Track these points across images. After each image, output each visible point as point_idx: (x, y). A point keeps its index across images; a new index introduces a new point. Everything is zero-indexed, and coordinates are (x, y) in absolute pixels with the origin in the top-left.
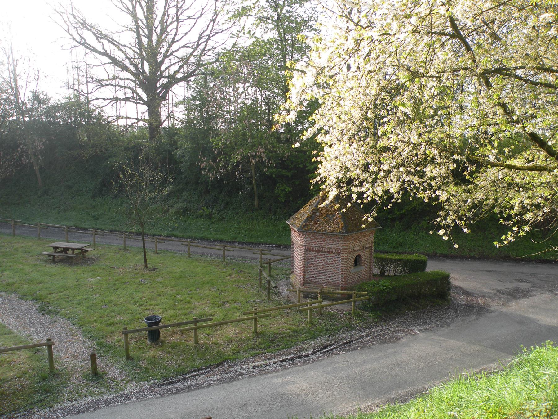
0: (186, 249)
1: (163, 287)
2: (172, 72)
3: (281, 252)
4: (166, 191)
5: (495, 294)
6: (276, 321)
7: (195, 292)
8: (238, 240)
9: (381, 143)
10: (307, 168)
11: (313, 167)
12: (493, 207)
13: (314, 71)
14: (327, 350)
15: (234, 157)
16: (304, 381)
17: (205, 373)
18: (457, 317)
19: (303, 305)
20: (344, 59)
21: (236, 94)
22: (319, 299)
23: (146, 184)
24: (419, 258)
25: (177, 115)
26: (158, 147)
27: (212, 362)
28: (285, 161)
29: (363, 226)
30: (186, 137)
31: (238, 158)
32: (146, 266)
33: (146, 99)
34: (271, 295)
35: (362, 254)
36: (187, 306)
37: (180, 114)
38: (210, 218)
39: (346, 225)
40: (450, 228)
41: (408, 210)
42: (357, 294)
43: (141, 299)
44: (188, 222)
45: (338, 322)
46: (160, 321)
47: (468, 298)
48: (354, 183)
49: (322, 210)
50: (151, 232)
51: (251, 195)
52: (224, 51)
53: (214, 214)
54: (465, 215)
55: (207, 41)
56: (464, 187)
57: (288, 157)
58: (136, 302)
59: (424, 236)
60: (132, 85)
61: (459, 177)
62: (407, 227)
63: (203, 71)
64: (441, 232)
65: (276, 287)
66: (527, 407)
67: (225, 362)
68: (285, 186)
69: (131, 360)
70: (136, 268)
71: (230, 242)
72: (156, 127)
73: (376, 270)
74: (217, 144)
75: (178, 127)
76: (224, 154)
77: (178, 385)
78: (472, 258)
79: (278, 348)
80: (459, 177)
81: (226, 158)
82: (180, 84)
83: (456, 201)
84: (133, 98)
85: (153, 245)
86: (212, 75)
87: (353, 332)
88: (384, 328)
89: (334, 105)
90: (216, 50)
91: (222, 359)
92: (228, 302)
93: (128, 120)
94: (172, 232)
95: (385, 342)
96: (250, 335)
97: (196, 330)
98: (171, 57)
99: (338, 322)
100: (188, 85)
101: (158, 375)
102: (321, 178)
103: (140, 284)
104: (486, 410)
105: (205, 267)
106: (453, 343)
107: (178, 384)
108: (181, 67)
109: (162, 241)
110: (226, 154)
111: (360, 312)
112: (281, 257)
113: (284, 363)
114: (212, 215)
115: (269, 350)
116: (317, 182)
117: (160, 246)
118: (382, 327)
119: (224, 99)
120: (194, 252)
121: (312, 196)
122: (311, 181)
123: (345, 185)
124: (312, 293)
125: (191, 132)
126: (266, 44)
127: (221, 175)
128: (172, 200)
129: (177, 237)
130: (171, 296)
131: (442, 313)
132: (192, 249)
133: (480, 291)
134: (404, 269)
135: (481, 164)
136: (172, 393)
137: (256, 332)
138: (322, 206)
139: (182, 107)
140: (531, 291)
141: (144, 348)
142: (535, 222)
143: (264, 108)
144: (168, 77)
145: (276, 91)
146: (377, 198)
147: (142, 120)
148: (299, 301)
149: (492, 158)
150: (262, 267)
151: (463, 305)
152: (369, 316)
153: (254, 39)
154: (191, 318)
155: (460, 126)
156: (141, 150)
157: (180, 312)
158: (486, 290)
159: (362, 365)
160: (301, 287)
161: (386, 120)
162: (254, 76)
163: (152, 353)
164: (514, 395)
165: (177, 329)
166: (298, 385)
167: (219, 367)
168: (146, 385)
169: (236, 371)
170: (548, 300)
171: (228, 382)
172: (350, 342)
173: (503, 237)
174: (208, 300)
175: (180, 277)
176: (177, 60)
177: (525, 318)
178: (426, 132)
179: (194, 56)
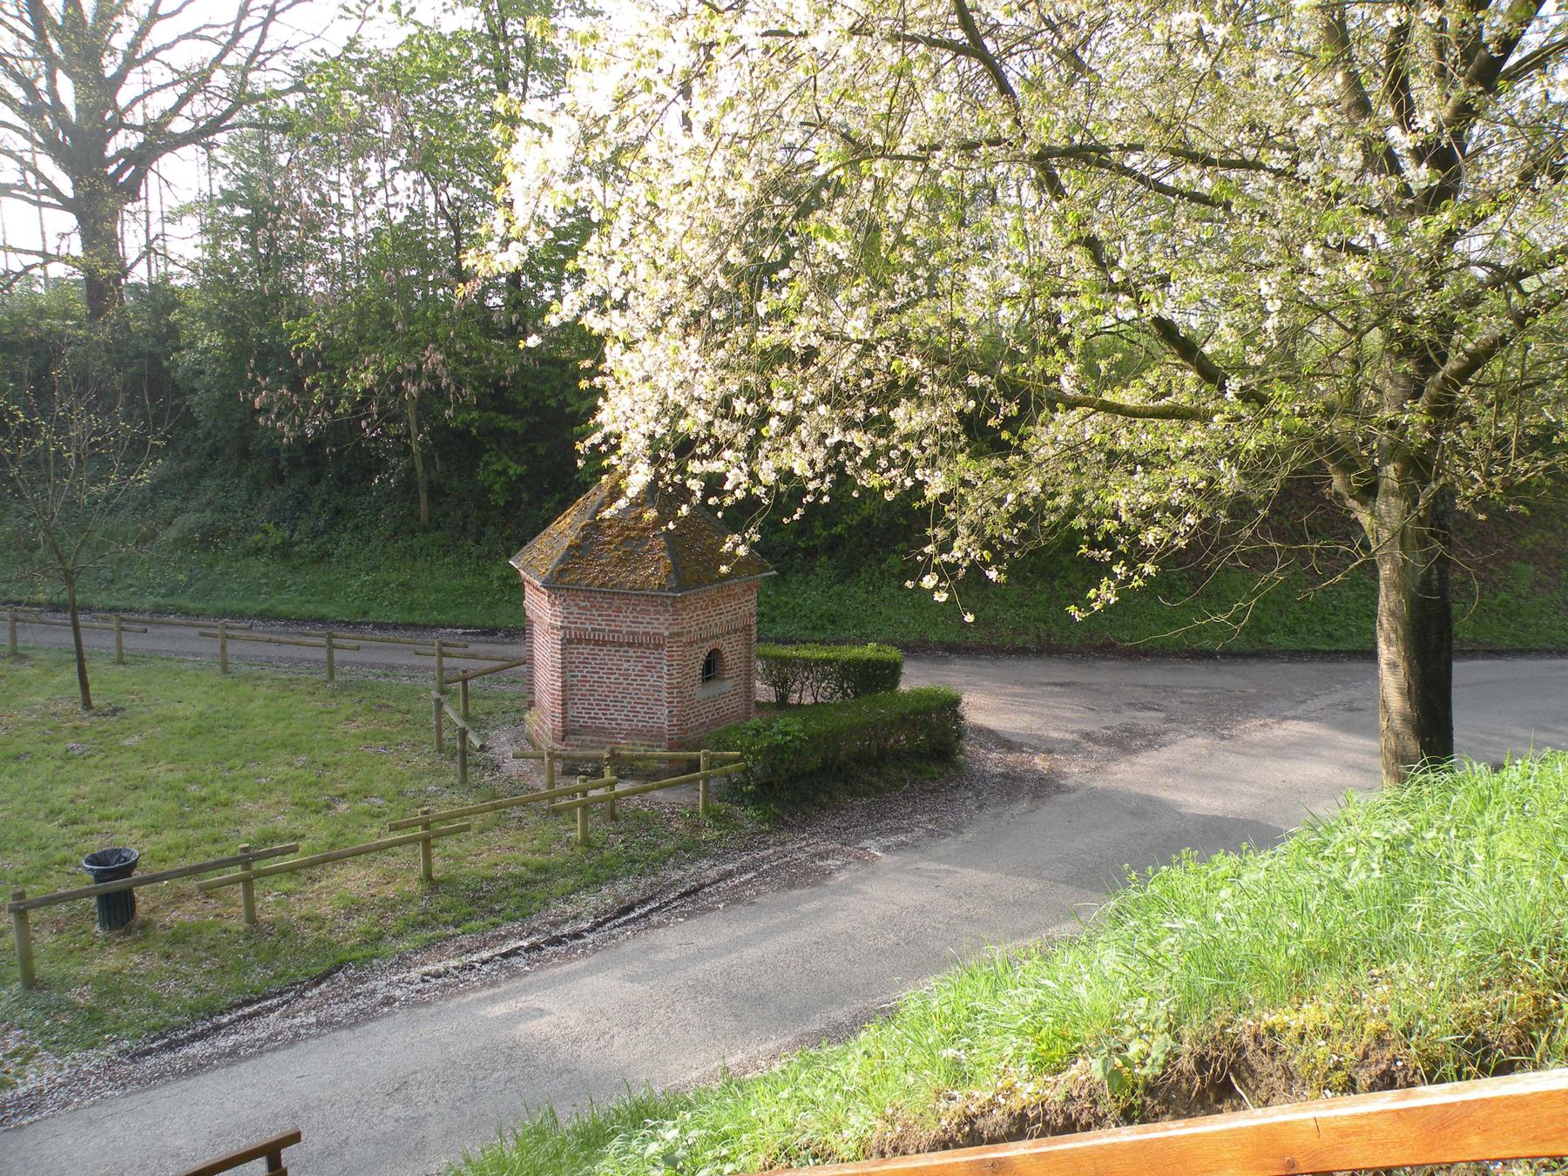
0: (214, 647)
1: (145, 762)
2: (154, 114)
3: (498, 648)
4: (145, 477)
5: (1076, 744)
6: (489, 843)
7: (245, 772)
8: (372, 616)
9: (766, 338)
10: (568, 410)
11: (586, 405)
12: (1072, 513)
13: (574, 126)
14: (633, 915)
15: (356, 378)
16: (586, 1009)
17: (279, 1006)
18: (980, 808)
19: (562, 794)
20: (664, 97)
21: (358, 192)
22: (608, 775)
23: (78, 455)
24: (881, 655)
25: (175, 247)
26: (117, 342)
27: (301, 973)
28: (505, 388)
29: (724, 569)
30: (206, 315)
31: (368, 378)
32: (87, 704)
33: (70, 194)
34: (469, 770)
35: (726, 649)
36: (221, 814)
37: (186, 244)
38: (286, 556)
39: (677, 569)
40: (962, 572)
41: (850, 527)
42: (712, 758)
43: (72, 801)
44: (218, 569)
45: (664, 837)
46: (134, 865)
47: (1011, 758)
48: (698, 451)
49: (610, 527)
50: (101, 599)
51: (408, 485)
52: (320, 60)
53: (297, 544)
54: (1001, 537)
55: (265, 24)
56: (996, 463)
57: (514, 377)
58: (54, 813)
59: (893, 596)
60: (19, 143)
61: (979, 436)
62: (848, 573)
63: (256, 115)
64: (929, 581)
65: (482, 748)
66: (1126, 1016)
67: (339, 969)
68: (506, 459)
69: (40, 989)
70: (52, 709)
71: (349, 623)
72: (107, 281)
73: (764, 691)
74: (307, 336)
75: (180, 283)
76: (325, 367)
77: (197, 1049)
78: (1021, 652)
79: (492, 919)
80: (979, 436)
81: (330, 379)
82: (181, 151)
83: (976, 500)
84: (25, 186)
85: (110, 641)
86: (284, 129)
87: (705, 863)
88: (789, 847)
89: (640, 229)
90: (296, 56)
91: (327, 966)
92: (343, 796)
93: (11, 255)
94: (169, 601)
95: (791, 885)
96: (414, 887)
97: (247, 882)
98: (149, 66)
99: (664, 837)
100: (211, 159)
101: (131, 1024)
102: (606, 440)
103: (67, 757)
104: (1033, 1034)
105: (274, 699)
106: (970, 876)
107: (197, 1044)
108: (184, 100)
109: (137, 627)
110: (332, 367)
111: (723, 807)
112: (497, 664)
113: (513, 960)
114: (292, 545)
115: (468, 926)
116: (594, 447)
117: (130, 641)
118: (783, 844)
119: (323, 202)
120: (238, 658)
121: (584, 488)
122: (579, 446)
123: (672, 456)
124: (588, 760)
125: (221, 301)
126: (448, 45)
127: (316, 428)
128: (167, 506)
129: (186, 613)
130: (169, 787)
131: (942, 799)
132: (233, 648)
133: (1039, 738)
134: (841, 687)
135: (1034, 400)
136: (178, 1075)
137: (428, 876)
138: (607, 514)
139: (191, 224)
140: (1165, 733)
141: (83, 949)
142: (1168, 550)
143: (443, 234)
144: (142, 129)
145: (479, 186)
146: (759, 491)
147: (59, 259)
148: (551, 785)
149: (1067, 386)
150: (443, 692)
151: (994, 776)
152: (747, 816)
153: (413, 30)
154: (233, 850)
155: (985, 296)
156: (58, 351)
157: (199, 833)
158: (1055, 735)
159: (730, 952)
160: (556, 746)
161: (784, 274)
162: (413, 138)
163: (112, 960)
164: (1099, 990)
165: (192, 884)
166: (554, 1019)
167: (323, 986)
168: (94, 1059)
169: (374, 991)
170: (1204, 751)
171: (350, 1027)
172: (695, 891)
173: (1092, 594)
174: (285, 793)
175: (197, 732)
176: (169, 77)
177: (1151, 800)
178: (892, 311)
179: (225, 68)
